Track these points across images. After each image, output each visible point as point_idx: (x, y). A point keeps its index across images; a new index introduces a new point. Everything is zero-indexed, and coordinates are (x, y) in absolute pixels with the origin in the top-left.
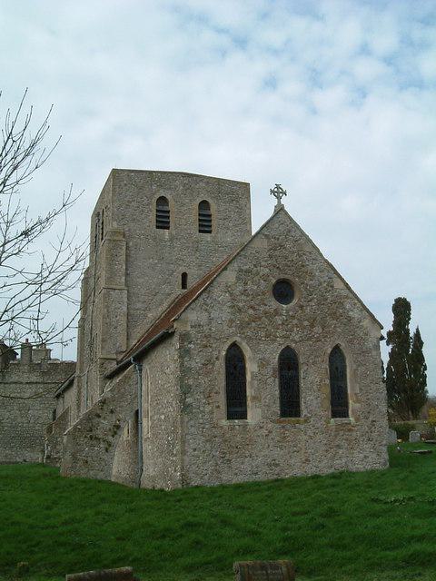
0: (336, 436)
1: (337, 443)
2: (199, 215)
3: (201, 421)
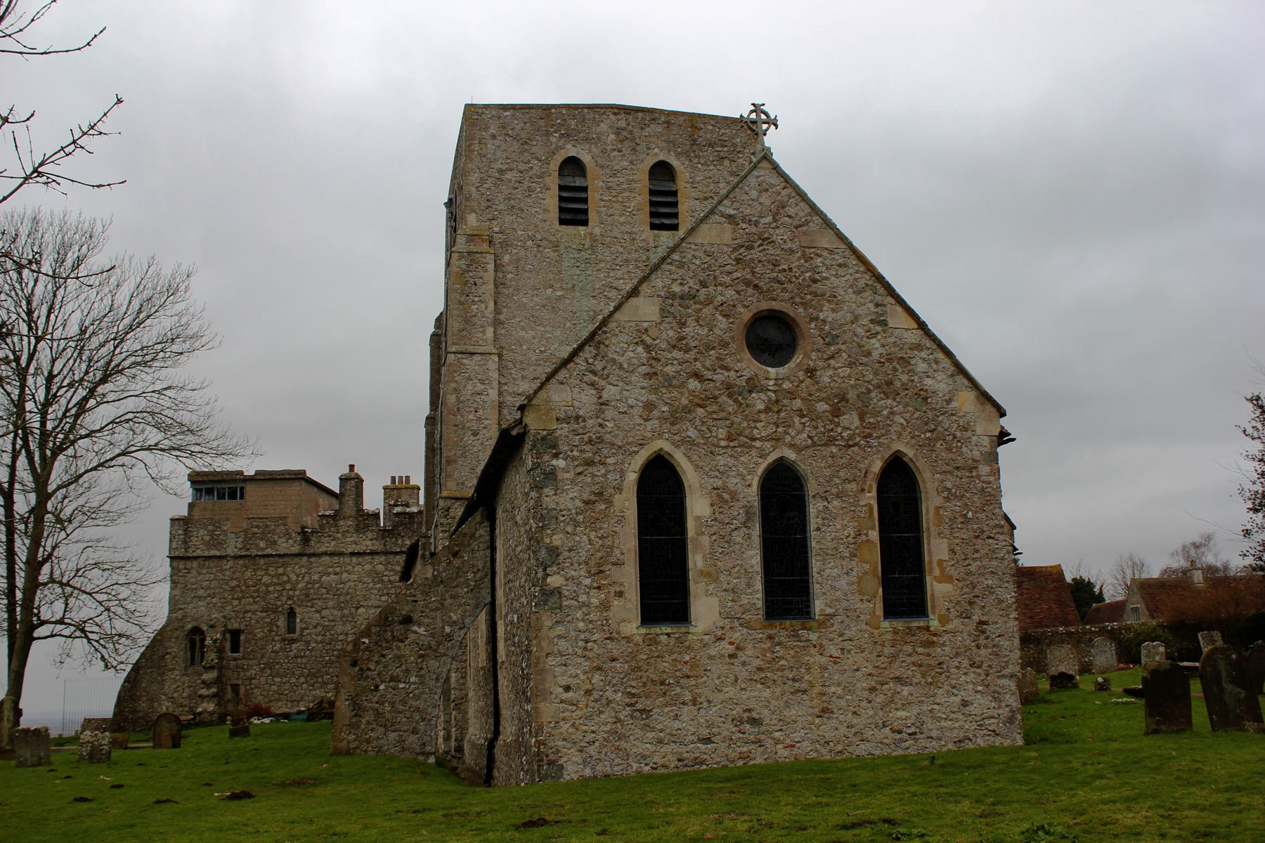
0: (894, 657)
1: (897, 674)
2: (652, 193)
3: (581, 625)
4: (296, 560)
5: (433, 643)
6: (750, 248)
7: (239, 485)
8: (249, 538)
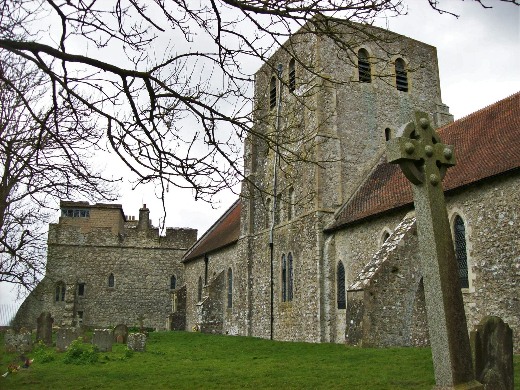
4: (115, 250)
5: (407, 284)
7: (86, 210)
8: (91, 236)
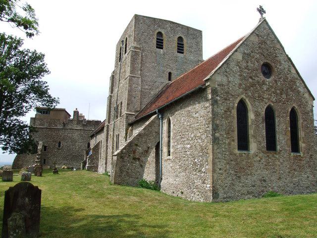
2: (178, 44)
6: (262, 44)
8: (50, 124)
